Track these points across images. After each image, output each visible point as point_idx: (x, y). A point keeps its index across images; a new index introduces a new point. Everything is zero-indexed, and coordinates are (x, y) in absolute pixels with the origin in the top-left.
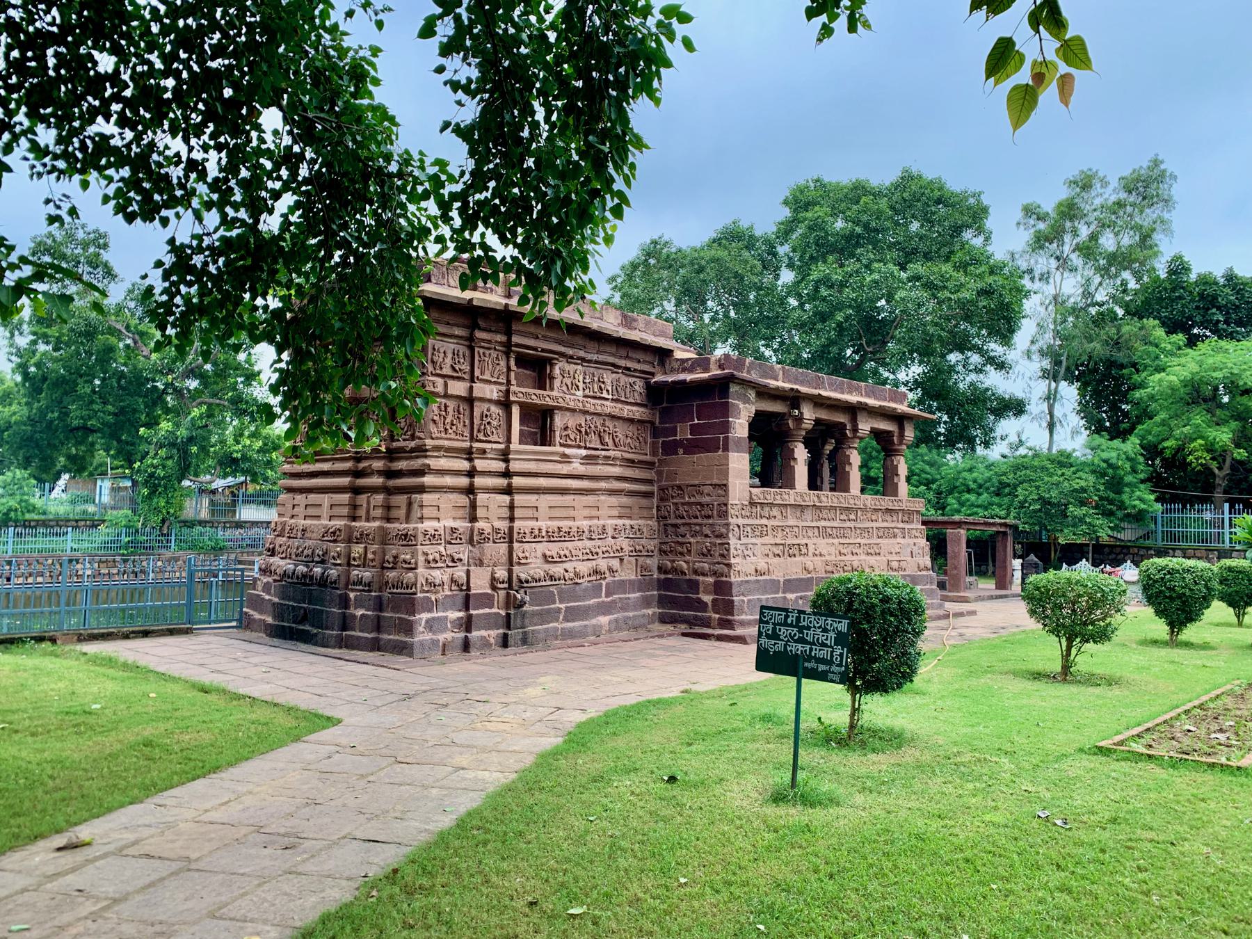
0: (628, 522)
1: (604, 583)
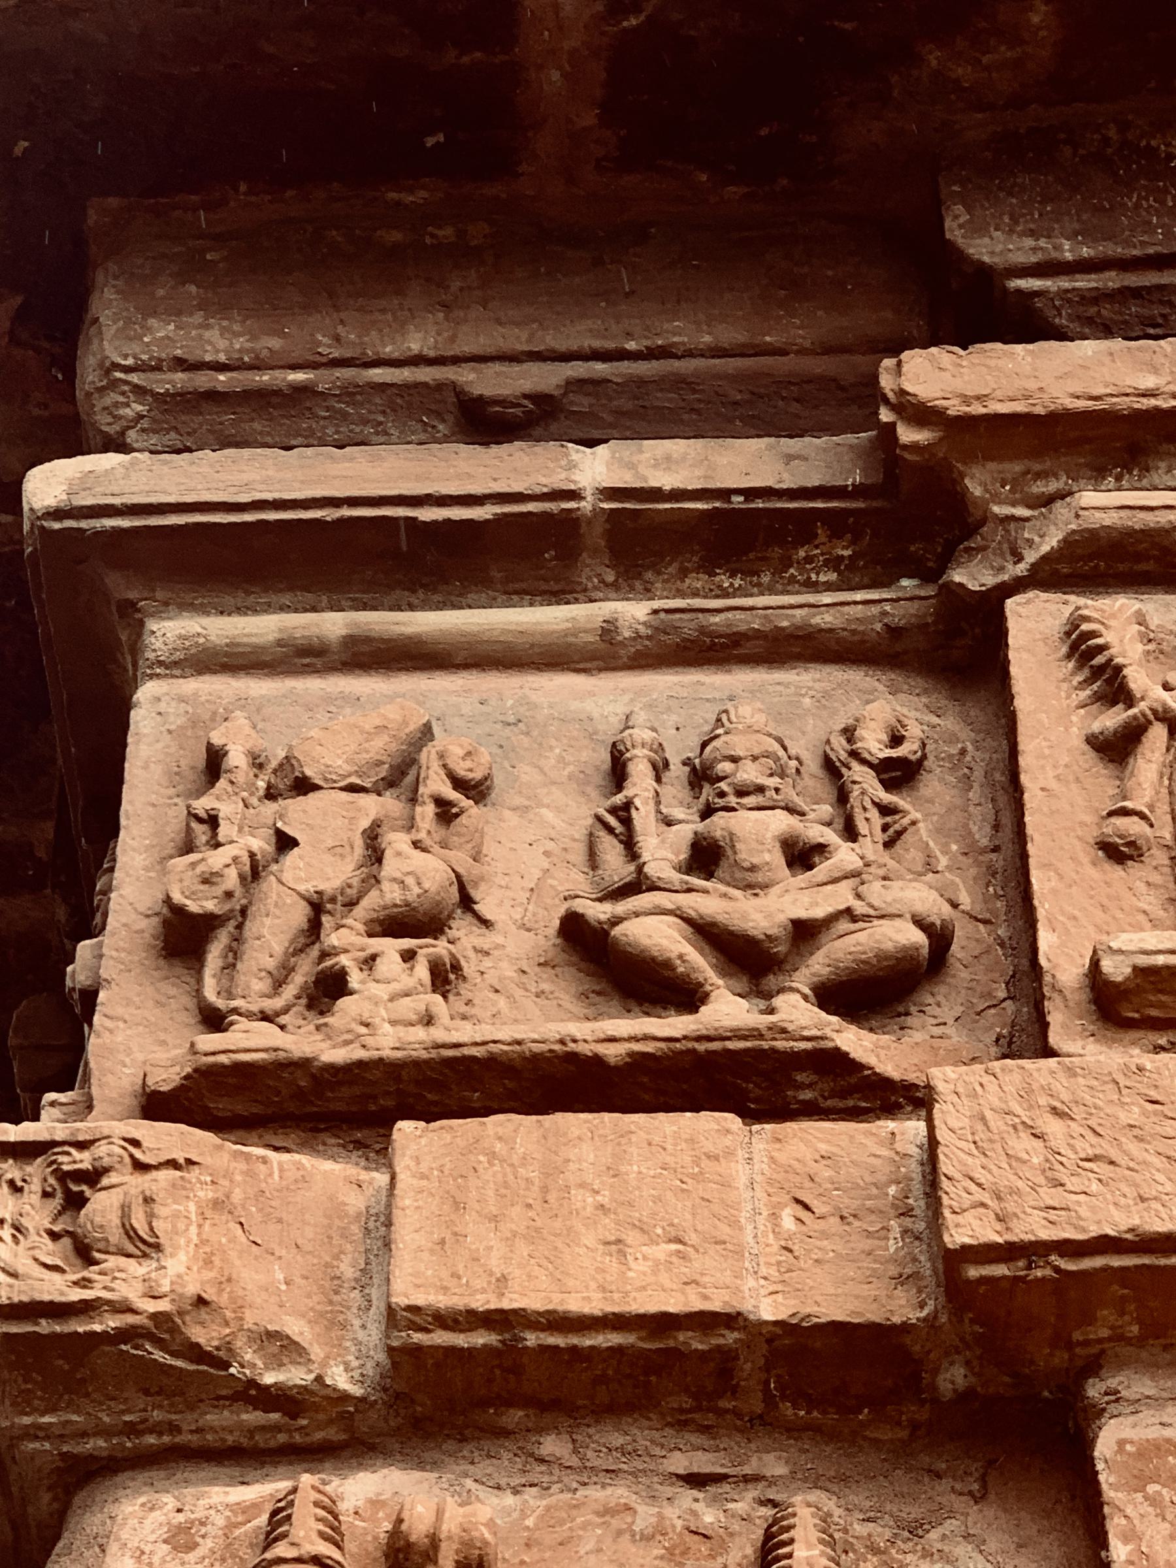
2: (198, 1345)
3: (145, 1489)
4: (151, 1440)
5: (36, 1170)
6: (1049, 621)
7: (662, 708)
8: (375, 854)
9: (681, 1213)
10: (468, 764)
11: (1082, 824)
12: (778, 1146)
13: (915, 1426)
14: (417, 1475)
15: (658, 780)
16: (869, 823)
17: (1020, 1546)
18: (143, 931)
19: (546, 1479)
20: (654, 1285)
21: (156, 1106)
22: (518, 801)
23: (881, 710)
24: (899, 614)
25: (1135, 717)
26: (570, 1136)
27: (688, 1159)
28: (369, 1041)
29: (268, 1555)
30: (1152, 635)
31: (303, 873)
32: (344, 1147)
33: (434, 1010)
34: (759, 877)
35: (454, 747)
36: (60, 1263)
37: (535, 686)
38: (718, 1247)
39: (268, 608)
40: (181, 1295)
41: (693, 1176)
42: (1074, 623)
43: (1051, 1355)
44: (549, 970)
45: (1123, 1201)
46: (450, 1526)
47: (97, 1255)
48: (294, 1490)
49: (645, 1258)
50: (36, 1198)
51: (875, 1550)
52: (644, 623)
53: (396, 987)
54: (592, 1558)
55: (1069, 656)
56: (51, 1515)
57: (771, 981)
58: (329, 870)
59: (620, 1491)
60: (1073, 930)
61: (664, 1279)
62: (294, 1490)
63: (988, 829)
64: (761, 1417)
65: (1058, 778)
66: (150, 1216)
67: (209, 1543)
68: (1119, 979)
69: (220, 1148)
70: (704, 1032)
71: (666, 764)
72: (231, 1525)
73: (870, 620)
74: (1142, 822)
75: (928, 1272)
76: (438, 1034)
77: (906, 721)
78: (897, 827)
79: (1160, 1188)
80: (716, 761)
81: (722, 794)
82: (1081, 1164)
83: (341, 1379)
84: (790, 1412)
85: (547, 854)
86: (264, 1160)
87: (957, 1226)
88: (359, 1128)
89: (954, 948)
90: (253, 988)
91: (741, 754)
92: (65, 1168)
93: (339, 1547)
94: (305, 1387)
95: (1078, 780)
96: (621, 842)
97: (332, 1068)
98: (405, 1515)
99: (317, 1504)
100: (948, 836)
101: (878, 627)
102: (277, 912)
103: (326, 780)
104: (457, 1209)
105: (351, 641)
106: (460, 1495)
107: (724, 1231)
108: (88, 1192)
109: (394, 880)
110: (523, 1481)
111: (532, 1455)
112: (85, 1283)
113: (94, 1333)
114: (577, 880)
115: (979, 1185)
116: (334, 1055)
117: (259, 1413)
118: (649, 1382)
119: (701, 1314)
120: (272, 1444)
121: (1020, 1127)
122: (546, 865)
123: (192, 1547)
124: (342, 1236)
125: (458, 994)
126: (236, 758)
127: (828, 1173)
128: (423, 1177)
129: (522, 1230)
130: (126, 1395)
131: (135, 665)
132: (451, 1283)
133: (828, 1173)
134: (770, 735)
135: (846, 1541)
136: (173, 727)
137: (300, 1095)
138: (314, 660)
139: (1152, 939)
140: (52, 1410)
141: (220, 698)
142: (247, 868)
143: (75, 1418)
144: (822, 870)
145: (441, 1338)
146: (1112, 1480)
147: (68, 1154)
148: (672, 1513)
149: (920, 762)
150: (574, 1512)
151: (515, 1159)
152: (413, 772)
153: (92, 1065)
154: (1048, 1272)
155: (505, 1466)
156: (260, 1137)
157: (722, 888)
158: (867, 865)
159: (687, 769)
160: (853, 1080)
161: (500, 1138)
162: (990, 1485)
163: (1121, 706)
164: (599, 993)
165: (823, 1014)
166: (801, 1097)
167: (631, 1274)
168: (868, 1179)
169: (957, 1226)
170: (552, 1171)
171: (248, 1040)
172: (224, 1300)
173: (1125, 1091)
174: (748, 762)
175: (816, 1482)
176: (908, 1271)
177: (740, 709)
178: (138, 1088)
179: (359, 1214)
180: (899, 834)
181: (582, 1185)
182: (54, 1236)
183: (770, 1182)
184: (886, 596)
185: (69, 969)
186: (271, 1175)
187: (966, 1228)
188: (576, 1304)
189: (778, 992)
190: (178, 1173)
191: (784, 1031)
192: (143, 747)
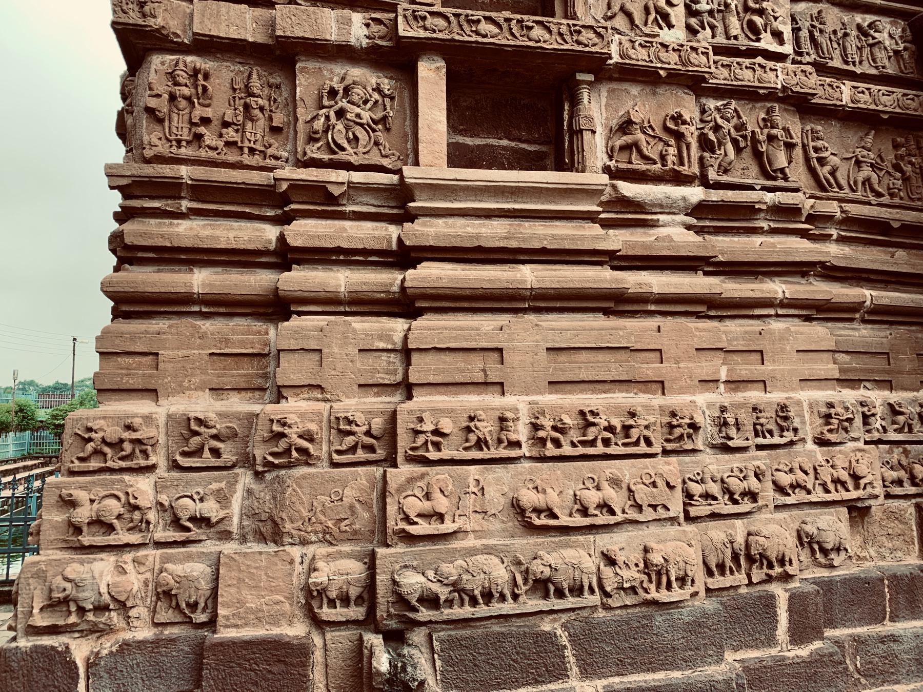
0: (878, 397)
1: (780, 592)
9: (238, 22)
20: (233, 33)
170: (218, 12)
175: (257, 65)
187: (279, 33)
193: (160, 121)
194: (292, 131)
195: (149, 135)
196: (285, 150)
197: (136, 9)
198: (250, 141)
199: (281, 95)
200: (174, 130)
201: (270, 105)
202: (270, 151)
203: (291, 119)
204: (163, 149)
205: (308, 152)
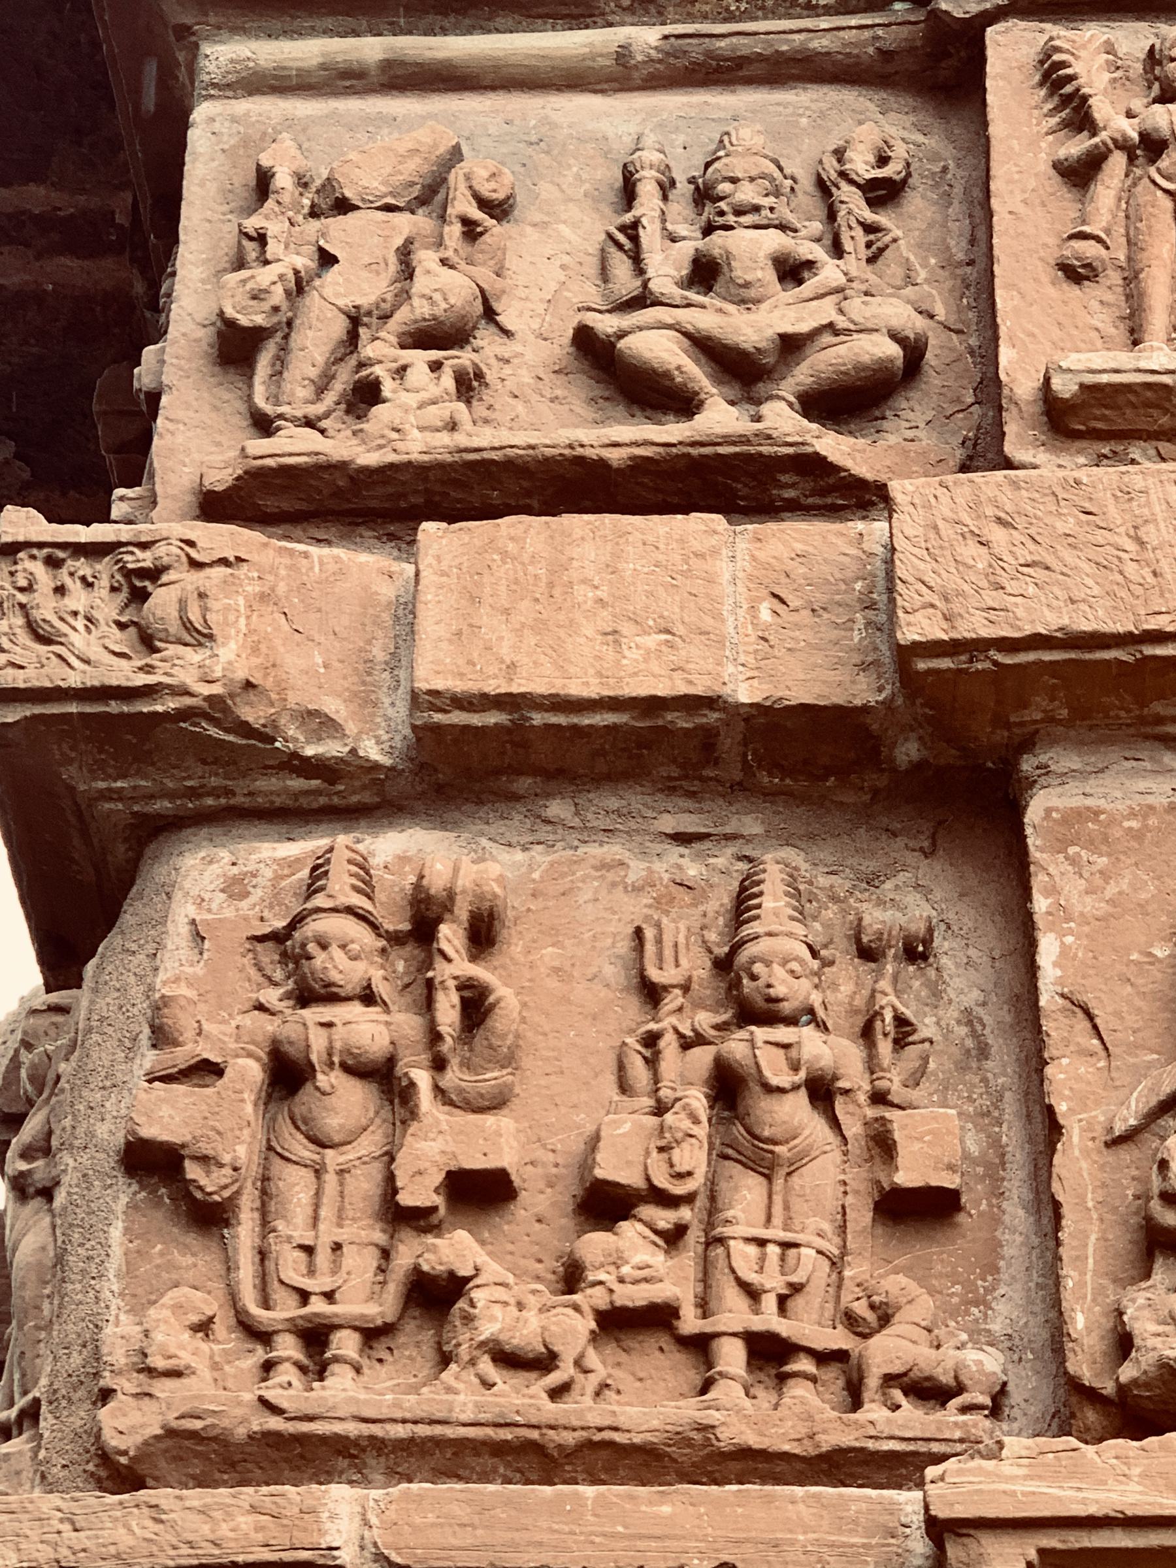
2: (247, 723)
3: (205, 843)
4: (210, 801)
5: (104, 568)
6: (1025, 50)
7: (667, 128)
8: (407, 272)
10: (493, 185)
11: (1045, 245)
12: (759, 545)
13: (876, 792)
14: (438, 834)
15: (665, 198)
16: (854, 241)
17: (961, 895)
18: (200, 340)
19: (551, 837)
20: (646, 670)
21: (214, 506)
22: (538, 217)
23: (870, 129)
24: (891, 38)
25: (1096, 146)
26: (575, 536)
27: (677, 558)
28: (399, 445)
29: (309, 905)
30: (1120, 63)
31: (344, 288)
32: (378, 538)
33: (457, 417)
34: (752, 293)
35: (479, 171)
36: (126, 650)
37: (557, 106)
38: (703, 638)
39: (313, 32)
40: (231, 680)
41: (682, 573)
42: (1048, 52)
43: (992, 733)
44: (562, 376)
45: (1055, 603)
46: (464, 882)
47: (158, 644)
48: (331, 850)
49: (638, 647)
50: (105, 593)
51: (834, 899)
52: (656, 48)
53: (425, 396)
54: (590, 906)
55: (1041, 84)
56: (127, 861)
57: (761, 388)
58: (365, 286)
59: (617, 848)
60: (1031, 346)
61: (655, 666)
62: (331, 850)
63: (964, 244)
64: (740, 784)
65: (1025, 202)
66: (205, 610)
67: (259, 893)
68: (1067, 396)
69: (265, 545)
70: (698, 438)
71: (673, 183)
72: (278, 878)
73: (865, 43)
74: (1099, 246)
75: (887, 660)
76: (461, 439)
77: (892, 142)
78: (879, 244)
79: (1088, 591)
80: (717, 182)
81: (722, 213)
82: (1025, 570)
83: (372, 751)
84: (766, 780)
85: (563, 267)
86: (306, 555)
87: (909, 624)
88: (392, 522)
89: (928, 355)
90: (298, 396)
91: (740, 175)
92: (130, 566)
93: (369, 898)
94: (341, 759)
95: (1043, 204)
96: (630, 257)
97: (366, 470)
98: (426, 872)
99: (350, 862)
100: (928, 250)
101: (871, 50)
102: (319, 325)
103: (363, 200)
104: (473, 602)
105: (388, 65)
106: (476, 851)
107: (708, 622)
108: (150, 588)
109: (423, 296)
110: (531, 839)
111: (539, 817)
112: (148, 669)
113: (156, 713)
114: (591, 293)
115: (930, 588)
116: (369, 458)
117: (302, 780)
118: (642, 755)
119: (686, 697)
120: (315, 805)
121: (968, 535)
122: (563, 279)
123: (246, 895)
124: (374, 623)
125: (481, 400)
126: (283, 180)
127: (802, 570)
128: (444, 574)
129: (530, 622)
130: (186, 764)
131: (192, 83)
132: (466, 669)
133: (802, 570)
134: (766, 157)
135: (811, 892)
136: (226, 147)
137: (338, 493)
138: (354, 82)
139: (1099, 360)
140: (123, 776)
141: (269, 118)
142: (292, 285)
143: (143, 783)
144: (811, 285)
145: (458, 718)
146: (1038, 843)
147: (132, 553)
148: (659, 867)
149: (904, 181)
150: (575, 867)
151: (526, 558)
152: (443, 191)
153: (156, 464)
154: (988, 665)
155: (516, 824)
156: (304, 531)
157: (718, 303)
158: (850, 280)
159: (692, 187)
160: (831, 481)
161: (512, 539)
162: (939, 842)
163: (1085, 133)
164: (607, 399)
165: (805, 422)
166: (786, 496)
167: (625, 662)
168: (838, 576)
169: (909, 624)
170: (558, 568)
171: (293, 445)
172: (269, 683)
173: (1063, 503)
174: (746, 183)
176: (870, 659)
177: (741, 132)
178: (196, 485)
179: (390, 603)
180: (881, 250)
181: (584, 581)
182: (122, 626)
183: (750, 578)
184: (877, 21)
185: (136, 371)
186: (312, 568)
187: (918, 627)
188: (576, 689)
189: (767, 399)
190: (229, 571)
191: (769, 437)
192: (198, 165)
193: (209, 1217)
194: (1016, 1212)
195: (138, 1307)
196: (980, 1337)
197: (107, 607)
198: (753, 1293)
199: (936, 992)
200: (291, 1266)
201: (872, 1065)
202: (885, 1352)
203: (1012, 1135)
204: (223, 1388)
205: (1143, 1325)
